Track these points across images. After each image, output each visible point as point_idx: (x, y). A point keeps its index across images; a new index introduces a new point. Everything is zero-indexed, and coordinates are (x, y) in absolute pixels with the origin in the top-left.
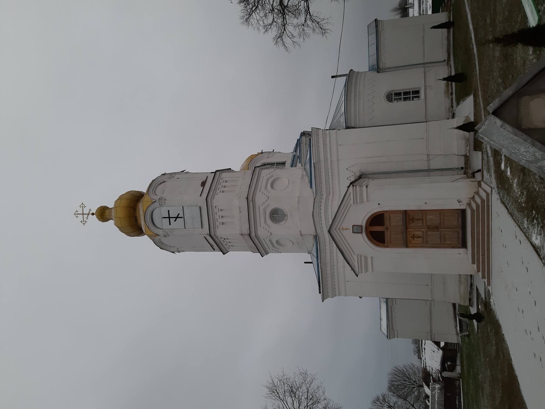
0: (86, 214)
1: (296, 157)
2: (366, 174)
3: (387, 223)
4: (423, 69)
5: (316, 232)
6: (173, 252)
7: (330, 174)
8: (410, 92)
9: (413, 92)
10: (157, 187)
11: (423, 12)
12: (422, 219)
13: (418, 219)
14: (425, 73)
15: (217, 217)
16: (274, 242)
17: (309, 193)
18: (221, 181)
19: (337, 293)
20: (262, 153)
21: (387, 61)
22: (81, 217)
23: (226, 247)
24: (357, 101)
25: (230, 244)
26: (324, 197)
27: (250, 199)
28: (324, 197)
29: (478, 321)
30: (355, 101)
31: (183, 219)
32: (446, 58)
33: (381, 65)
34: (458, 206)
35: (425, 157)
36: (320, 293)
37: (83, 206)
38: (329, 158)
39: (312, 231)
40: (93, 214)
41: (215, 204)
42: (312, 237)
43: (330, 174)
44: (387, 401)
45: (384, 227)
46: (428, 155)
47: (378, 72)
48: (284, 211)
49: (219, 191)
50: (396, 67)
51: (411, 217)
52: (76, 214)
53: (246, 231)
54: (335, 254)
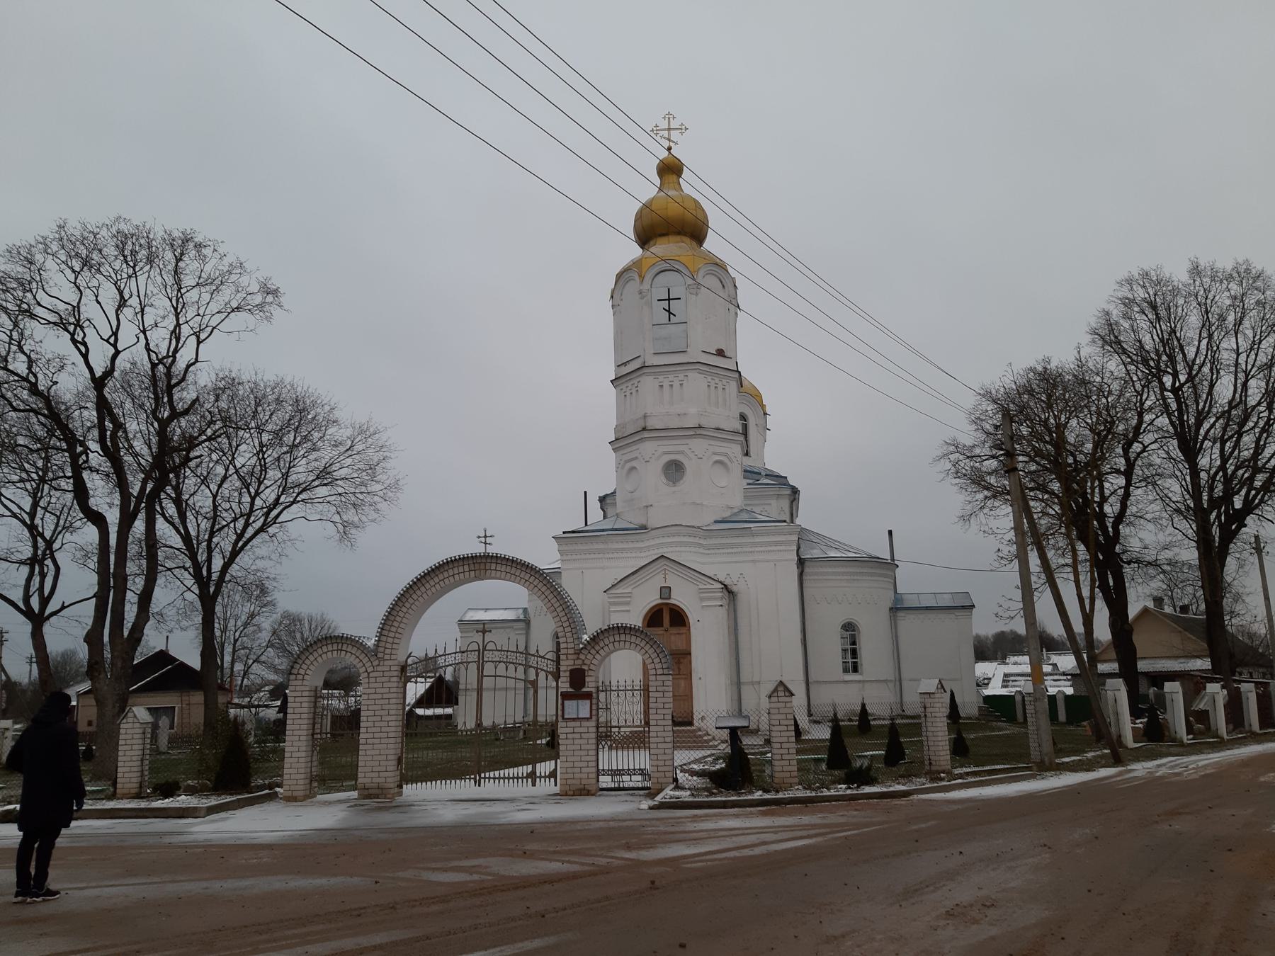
0: (669, 135)
1: (757, 477)
2: (734, 600)
3: (674, 630)
4: (893, 679)
5: (652, 529)
6: (612, 297)
7: (735, 550)
8: (856, 658)
9: (856, 663)
10: (716, 275)
11: (1013, 681)
12: (679, 674)
13: (679, 669)
14: (885, 681)
15: (671, 377)
16: (634, 464)
17: (706, 519)
18: (724, 381)
19: (565, 558)
20: (765, 414)
21: (908, 623)
22: (664, 125)
23: (624, 387)
24: (846, 577)
25: (628, 394)
26: (701, 541)
27: (699, 432)
28: (701, 541)
29: (548, 744)
30: (843, 574)
31: (668, 322)
32: (908, 713)
33: (901, 614)
34: (696, 716)
35: (756, 679)
36: (564, 533)
37: (683, 129)
38: (757, 549)
39: (652, 523)
40: (669, 149)
41: (690, 374)
42: (642, 521)
43: (735, 550)
44: (264, 609)
45: (668, 626)
46: (759, 683)
47: (891, 609)
48: (682, 482)
49: (710, 380)
50: (897, 637)
51: (682, 660)
52: (669, 117)
53: (651, 423)
54: (647, 553)
